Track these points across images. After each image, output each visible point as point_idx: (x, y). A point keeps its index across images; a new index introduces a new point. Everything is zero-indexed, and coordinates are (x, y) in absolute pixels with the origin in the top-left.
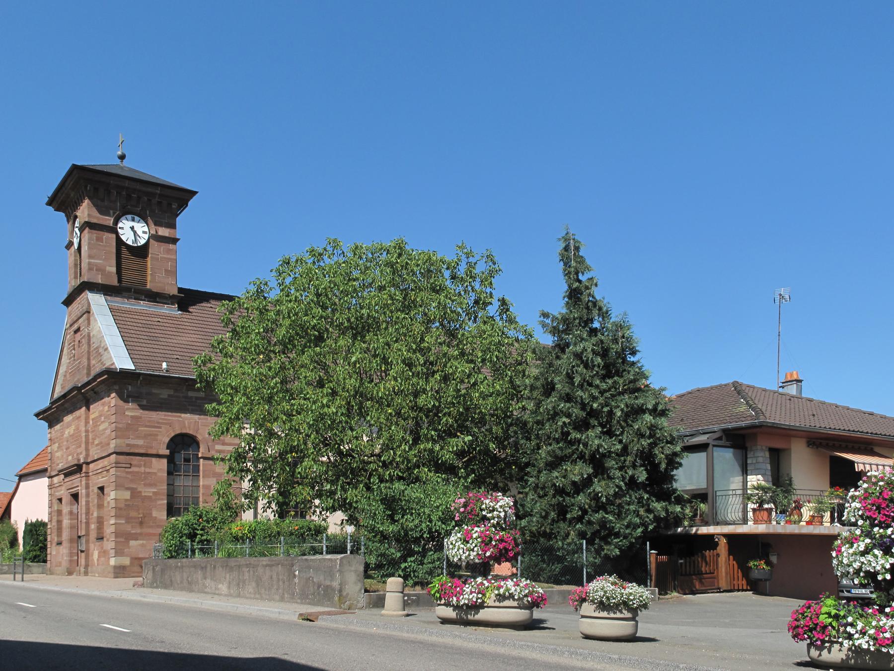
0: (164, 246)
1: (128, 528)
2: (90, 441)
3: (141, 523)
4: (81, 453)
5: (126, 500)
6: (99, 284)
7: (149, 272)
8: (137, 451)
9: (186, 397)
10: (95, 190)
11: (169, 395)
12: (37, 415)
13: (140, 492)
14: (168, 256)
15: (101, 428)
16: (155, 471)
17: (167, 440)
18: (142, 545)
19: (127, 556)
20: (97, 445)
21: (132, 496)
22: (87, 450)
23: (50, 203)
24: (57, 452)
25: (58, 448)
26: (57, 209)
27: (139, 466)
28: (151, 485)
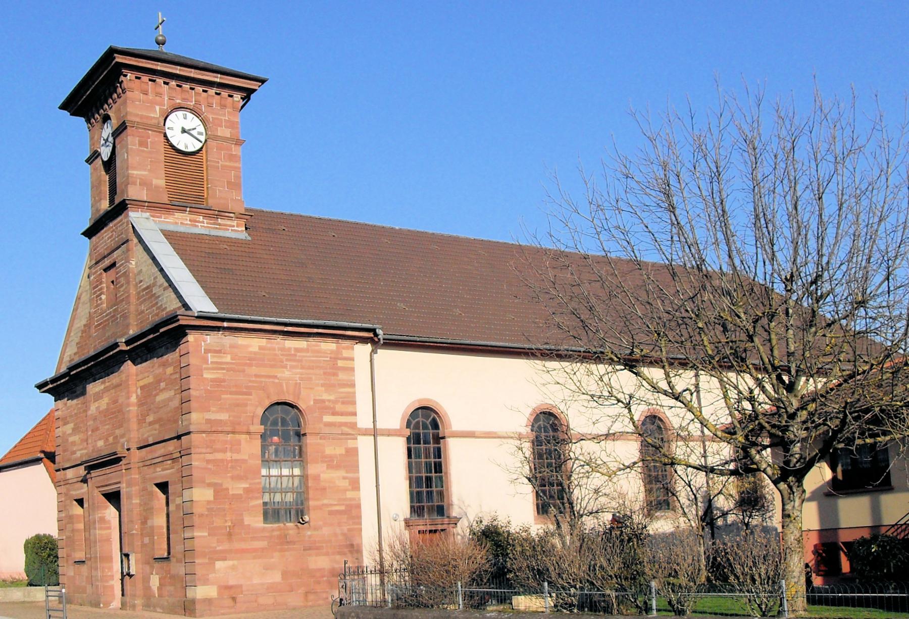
5: (209, 502)
11: (261, 348)
12: (40, 387)
13: (227, 489)
14: (232, 164)
15: (159, 398)
16: (246, 457)
18: (233, 568)
19: (212, 584)
20: (150, 424)
21: (216, 494)
23: (64, 106)
24: (70, 435)
26: (74, 114)
28: (239, 478)
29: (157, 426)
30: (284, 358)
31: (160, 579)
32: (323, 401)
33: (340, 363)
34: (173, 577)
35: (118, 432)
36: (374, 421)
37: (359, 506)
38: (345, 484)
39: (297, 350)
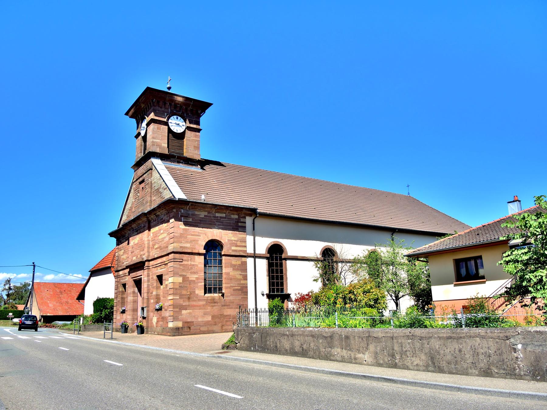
0: (193, 133)
1: (181, 302)
2: (151, 246)
3: (189, 298)
4: (144, 254)
5: (180, 283)
6: (158, 153)
7: (185, 147)
8: (186, 251)
9: (215, 217)
10: (152, 103)
11: (205, 216)
15: (160, 237)
17: (204, 244)
18: (190, 313)
19: (180, 321)
20: (156, 249)
21: (183, 280)
22: (148, 252)
25: (124, 253)
27: (188, 261)
29: (158, 250)
30: (215, 221)
31: (157, 319)
32: (232, 240)
33: (240, 224)
34: (163, 318)
35: (142, 253)
36: (255, 250)
37: (247, 287)
38: (241, 277)
39: (221, 217)
